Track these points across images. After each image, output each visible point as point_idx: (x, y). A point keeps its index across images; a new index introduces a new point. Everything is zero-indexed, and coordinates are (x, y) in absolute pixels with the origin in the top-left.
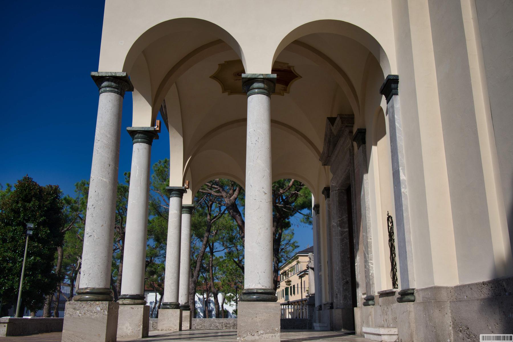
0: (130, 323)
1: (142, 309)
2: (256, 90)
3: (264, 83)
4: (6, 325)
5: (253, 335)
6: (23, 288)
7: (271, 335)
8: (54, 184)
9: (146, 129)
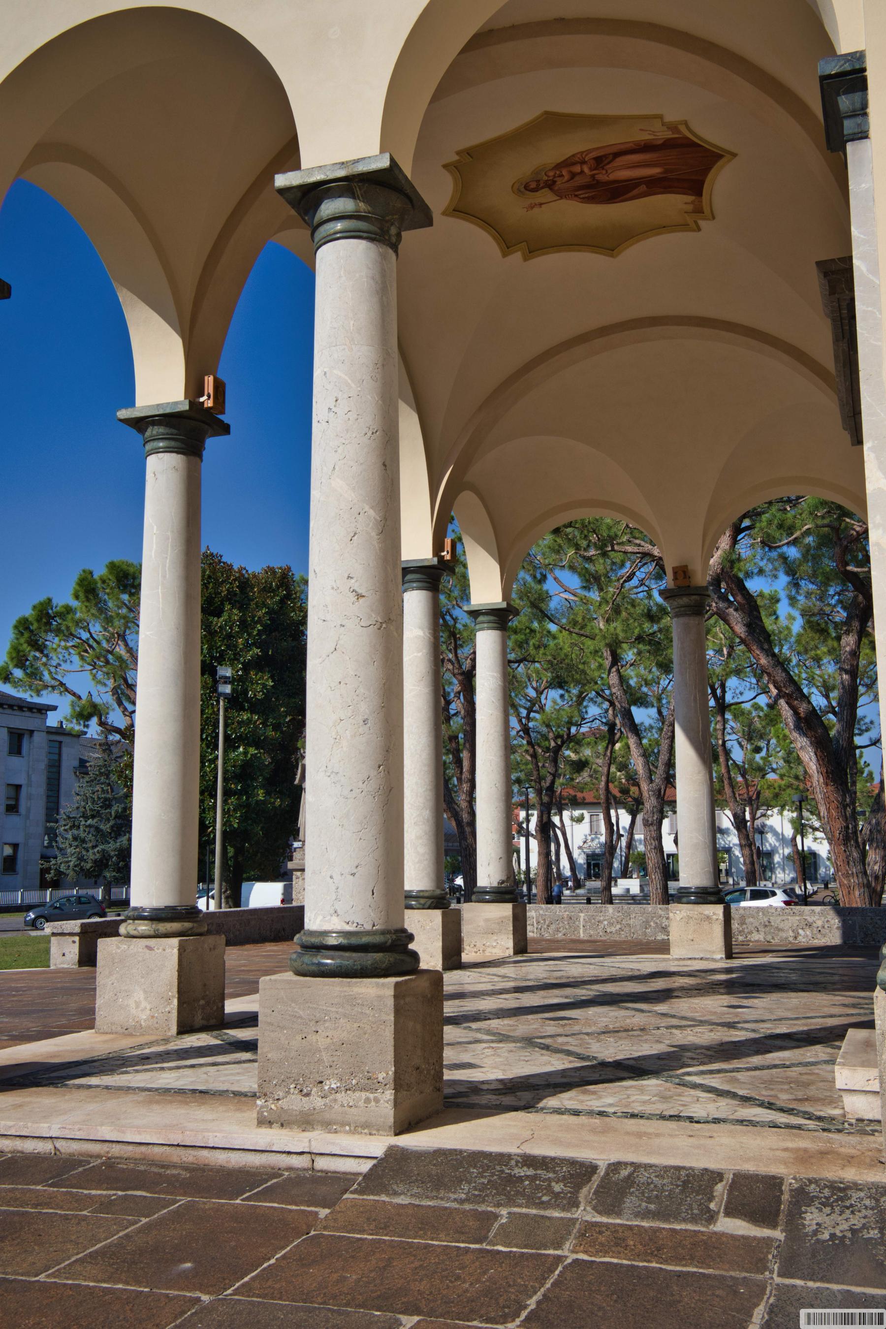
0: (145, 992)
1: (176, 951)
2: (339, 226)
3: (353, 196)
4: (77, 939)
5: (308, 1095)
6: (224, 824)
7: (364, 1095)
8: (278, 563)
9: (168, 411)
